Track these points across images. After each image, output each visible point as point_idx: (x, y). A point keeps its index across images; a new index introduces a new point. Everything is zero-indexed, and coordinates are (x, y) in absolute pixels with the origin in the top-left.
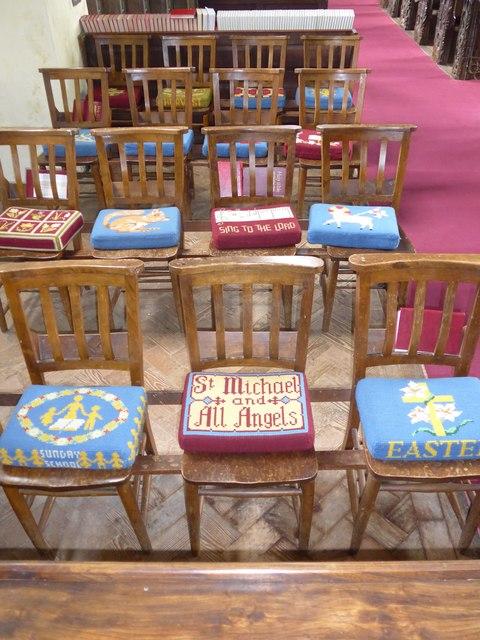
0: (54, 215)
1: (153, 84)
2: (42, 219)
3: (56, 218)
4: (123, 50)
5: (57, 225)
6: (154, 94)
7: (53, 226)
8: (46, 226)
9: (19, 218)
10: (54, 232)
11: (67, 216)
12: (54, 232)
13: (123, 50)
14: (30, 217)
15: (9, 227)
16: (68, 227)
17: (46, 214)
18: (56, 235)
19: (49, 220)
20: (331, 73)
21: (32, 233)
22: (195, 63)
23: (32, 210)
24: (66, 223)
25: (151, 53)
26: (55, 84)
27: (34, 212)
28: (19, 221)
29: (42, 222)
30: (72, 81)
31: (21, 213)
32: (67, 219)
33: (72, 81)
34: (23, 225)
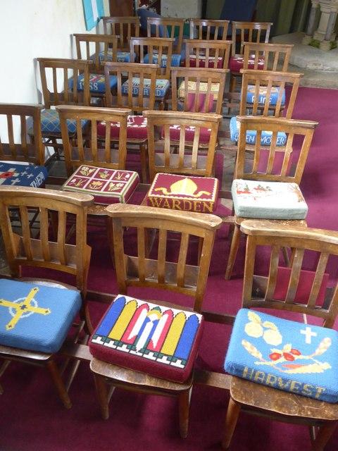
0: (116, 175)
1: (146, 47)
2: (108, 178)
3: (119, 178)
4: (163, 239)
5: (121, 185)
6: (146, 53)
7: (118, 185)
8: (112, 185)
9: (91, 175)
10: (119, 191)
11: (128, 176)
12: (119, 191)
13: (163, 239)
14: (98, 176)
15: (84, 184)
16: (130, 185)
17: (111, 173)
18: (121, 194)
19: (113, 179)
20: (259, 46)
21: (102, 191)
22: (177, 35)
23: (99, 169)
24: (128, 183)
25: (184, 30)
26: (49, 71)
27: (101, 171)
28: (91, 179)
29: (109, 181)
30: (62, 70)
31: (91, 171)
32: (128, 179)
33: (62, 70)
34: (94, 183)
